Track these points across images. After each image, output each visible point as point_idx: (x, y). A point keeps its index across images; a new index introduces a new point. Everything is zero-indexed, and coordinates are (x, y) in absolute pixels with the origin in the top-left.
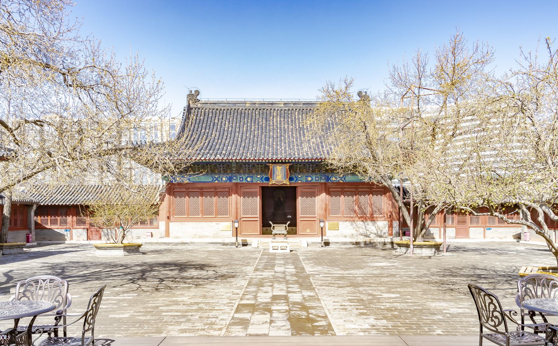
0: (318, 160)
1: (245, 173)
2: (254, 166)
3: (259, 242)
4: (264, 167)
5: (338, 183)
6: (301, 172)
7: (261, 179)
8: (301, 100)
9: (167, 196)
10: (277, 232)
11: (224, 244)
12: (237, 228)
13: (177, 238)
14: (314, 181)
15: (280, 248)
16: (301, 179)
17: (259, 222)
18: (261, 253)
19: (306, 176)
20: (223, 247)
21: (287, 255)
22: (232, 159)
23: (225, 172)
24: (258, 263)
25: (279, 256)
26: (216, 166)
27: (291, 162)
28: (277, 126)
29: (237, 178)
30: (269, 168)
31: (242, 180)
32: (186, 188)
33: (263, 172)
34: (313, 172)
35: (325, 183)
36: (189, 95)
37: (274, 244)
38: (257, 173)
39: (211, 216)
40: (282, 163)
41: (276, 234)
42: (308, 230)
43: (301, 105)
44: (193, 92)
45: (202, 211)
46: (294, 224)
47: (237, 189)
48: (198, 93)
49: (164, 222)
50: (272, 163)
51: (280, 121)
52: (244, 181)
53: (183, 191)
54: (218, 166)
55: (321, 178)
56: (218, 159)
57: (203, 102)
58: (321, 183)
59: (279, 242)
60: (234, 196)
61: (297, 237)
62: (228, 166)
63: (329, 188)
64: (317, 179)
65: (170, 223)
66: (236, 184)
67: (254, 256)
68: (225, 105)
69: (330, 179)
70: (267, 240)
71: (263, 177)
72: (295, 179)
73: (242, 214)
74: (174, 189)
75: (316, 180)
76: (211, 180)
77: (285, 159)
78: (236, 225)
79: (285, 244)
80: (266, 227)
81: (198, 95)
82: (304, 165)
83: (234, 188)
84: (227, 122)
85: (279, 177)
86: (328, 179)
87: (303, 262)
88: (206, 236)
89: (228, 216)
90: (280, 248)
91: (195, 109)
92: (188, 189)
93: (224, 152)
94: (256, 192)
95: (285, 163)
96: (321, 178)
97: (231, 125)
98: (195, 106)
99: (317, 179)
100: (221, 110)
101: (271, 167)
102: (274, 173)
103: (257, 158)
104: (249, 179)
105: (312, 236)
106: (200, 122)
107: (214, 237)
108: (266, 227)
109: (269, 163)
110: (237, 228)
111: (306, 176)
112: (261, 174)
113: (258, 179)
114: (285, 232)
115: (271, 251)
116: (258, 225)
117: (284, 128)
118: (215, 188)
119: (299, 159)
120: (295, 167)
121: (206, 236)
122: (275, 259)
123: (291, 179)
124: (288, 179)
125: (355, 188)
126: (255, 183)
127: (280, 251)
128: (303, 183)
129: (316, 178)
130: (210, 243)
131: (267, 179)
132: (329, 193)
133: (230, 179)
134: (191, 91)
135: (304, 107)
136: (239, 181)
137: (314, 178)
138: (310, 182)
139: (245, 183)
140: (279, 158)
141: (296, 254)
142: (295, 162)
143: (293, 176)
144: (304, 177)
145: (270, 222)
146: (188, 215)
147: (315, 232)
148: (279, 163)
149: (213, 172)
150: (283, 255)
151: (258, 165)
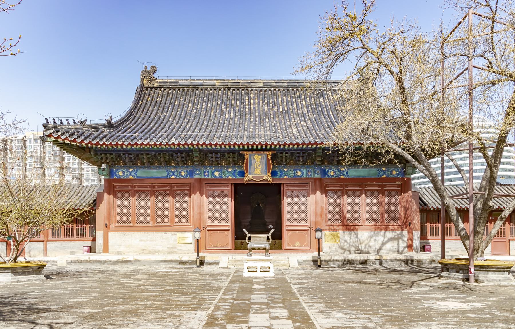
0: (312, 145)
1: (211, 165)
2: (223, 156)
3: (226, 260)
4: (236, 156)
5: (338, 179)
6: (287, 164)
7: (234, 173)
8: (285, 79)
9: (106, 195)
10: (255, 246)
11: (181, 263)
12: (198, 240)
13: (119, 253)
14: (305, 176)
15: (259, 270)
16: (287, 173)
18: (230, 278)
19: (294, 170)
20: (179, 266)
21: (270, 281)
22: (192, 144)
23: (185, 164)
24: (221, 300)
25: (259, 283)
26: (172, 156)
27: (275, 149)
28: (254, 108)
29: (201, 173)
30: (244, 158)
31: (208, 175)
32: (132, 187)
33: (235, 164)
34: (304, 164)
35: (320, 180)
36: (143, 72)
37: (251, 264)
38: (228, 165)
39: (165, 224)
40: (262, 150)
41: (253, 249)
42: (298, 244)
43: (286, 84)
44: (149, 69)
45: (153, 217)
46: (278, 236)
47: (201, 186)
48: (154, 69)
49: (102, 232)
50: (248, 150)
51: (259, 102)
52: (210, 177)
53: (127, 191)
54: (175, 155)
55: (314, 172)
56: (173, 144)
57: (161, 80)
58: (315, 179)
59: (258, 262)
60: (196, 197)
61: (283, 252)
62: (189, 155)
63: (326, 186)
64: (309, 173)
65: (110, 235)
66: (200, 180)
67: (216, 284)
68: (189, 84)
69: (326, 173)
70: (241, 256)
71: (235, 171)
72: (279, 174)
73: (207, 221)
74: (115, 187)
75: (308, 175)
76: (165, 175)
77: (266, 144)
78: (197, 235)
79: (267, 264)
80: (240, 240)
81: (155, 72)
82: (292, 154)
83: (197, 185)
84: (190, 105)
85: (258, 170)
86: (324, 173)
87: (300, 298)
88: (158, 252)
89: (189, 224)
90: (259, 270)
91: (151, 89)
92: (135, 187)
93: (182, 136)
94: (226, 191)
95: (266, 150)
96: (314, 172)
97: (195, 106)
99: (309, 173)
100: (184, 90)
101: (246, 157)
102: (251, 165)
103: (226, 143)
104: (216, 174)
105: (303, 252)
106: (155, 104)
107: (169, 253)
108: (240, 240)
109: (244, 150)
110: (198, 240)
111: (294, 170)
112: (233, 167)
113: (230, 174)
114: (268, 246)
115: (246, 274)
116: (230, 235)
117: (264, 110)
118: (171, 186)
119: (285, 144)
120: (281, 156)
121: (158, 252)
122: (250, 291)
123: (274, 173)
124: (270, 174)
125: (361, 186)
126: (225, 180)
127: (259, 274)
128: (291, 179)
129: (308, 172)
130: (162, 261)
131: (242, 174)
132: (325, 192)
133: (192, 173)
134: (146, 68)
135: (290, 86)
136: (203, 177)
138: (300, 178)
139: (212, 179)
140: (257, 143)
141: (285, 279)
142: (280, 149)
143: (277, 169)
144: (292, 171)
145: (245, 230)
146: (134, 222)
147: (307, 245)
148: (257, 149)
149: (168, 164)
150: (266, 281)
151: (229, 154)
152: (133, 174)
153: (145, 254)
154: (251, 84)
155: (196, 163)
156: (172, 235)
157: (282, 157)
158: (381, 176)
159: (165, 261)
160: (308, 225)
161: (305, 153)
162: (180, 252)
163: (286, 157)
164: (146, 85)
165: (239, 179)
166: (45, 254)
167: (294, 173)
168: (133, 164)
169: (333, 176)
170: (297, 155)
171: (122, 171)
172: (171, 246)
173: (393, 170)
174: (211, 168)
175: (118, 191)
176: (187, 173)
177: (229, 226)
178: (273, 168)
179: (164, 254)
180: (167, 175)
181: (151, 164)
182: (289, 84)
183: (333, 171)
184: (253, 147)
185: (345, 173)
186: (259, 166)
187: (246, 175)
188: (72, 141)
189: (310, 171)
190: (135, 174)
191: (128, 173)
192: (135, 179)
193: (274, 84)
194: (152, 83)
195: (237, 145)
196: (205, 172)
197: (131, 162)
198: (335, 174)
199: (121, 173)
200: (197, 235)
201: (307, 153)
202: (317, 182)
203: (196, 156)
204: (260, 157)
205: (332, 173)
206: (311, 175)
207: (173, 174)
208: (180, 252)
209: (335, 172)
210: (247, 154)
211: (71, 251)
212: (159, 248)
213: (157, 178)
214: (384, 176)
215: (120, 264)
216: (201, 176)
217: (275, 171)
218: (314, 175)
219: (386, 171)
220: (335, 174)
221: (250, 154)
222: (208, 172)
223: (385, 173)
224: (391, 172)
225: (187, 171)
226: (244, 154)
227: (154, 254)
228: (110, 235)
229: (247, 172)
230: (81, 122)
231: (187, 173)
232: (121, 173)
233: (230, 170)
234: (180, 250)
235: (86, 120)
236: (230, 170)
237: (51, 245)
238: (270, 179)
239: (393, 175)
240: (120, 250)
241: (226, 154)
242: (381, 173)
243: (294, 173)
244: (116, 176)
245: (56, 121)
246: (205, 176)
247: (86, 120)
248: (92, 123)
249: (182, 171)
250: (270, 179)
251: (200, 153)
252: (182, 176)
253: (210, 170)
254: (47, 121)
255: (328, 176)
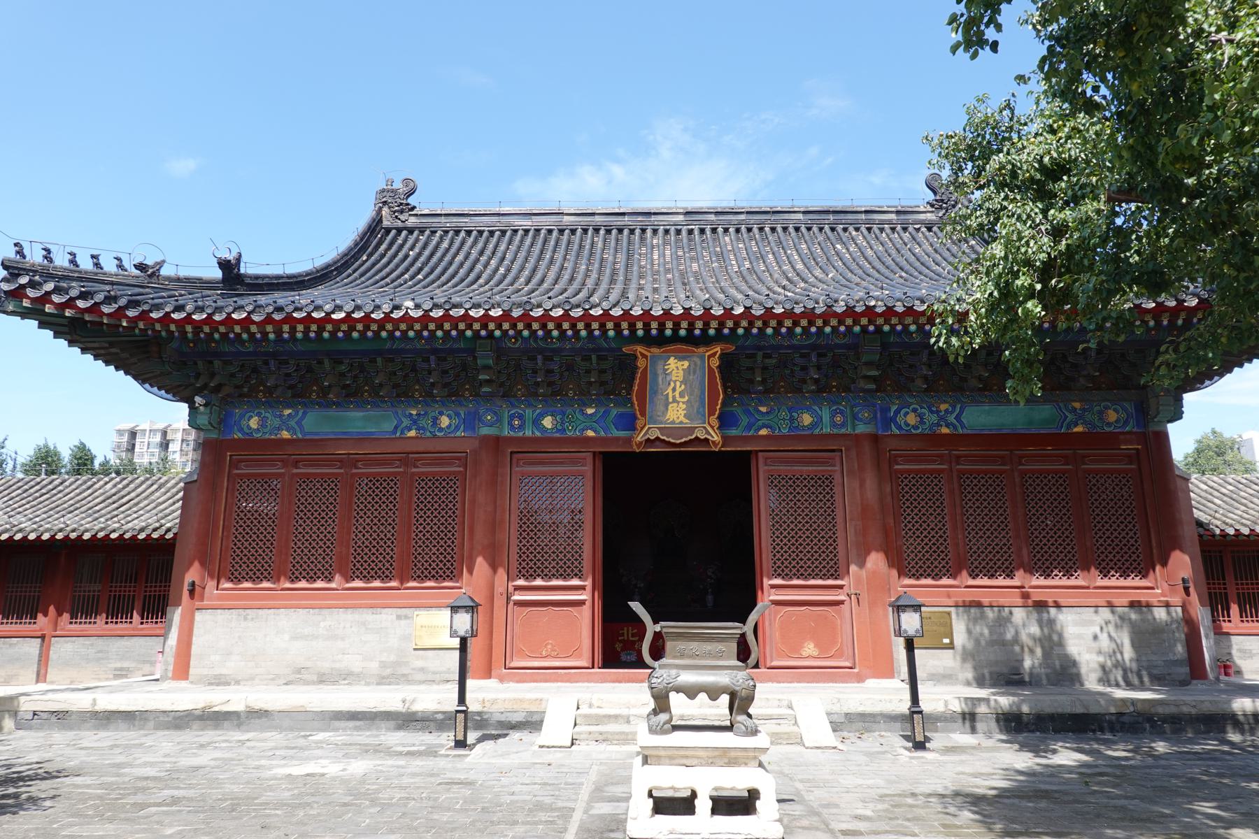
5: (934, 439)
6: (767, 391)
16: (764, 423)
17: (586, 609)
19: (790, 410)
31: (521, 427)
32: (285, 463)
35: (875, 439)
36: (383, 191)
37: (673, 780)
40: (691, 340)
42: (810, 649)
43: (742, 217)
50: (648, 341)
52: (528, 433)
55: (855, 417)
57: (426, 212)
58: (857, 438)
63: (893, 460)
64: (838, 419)
65: (199, 616)
66: (496, 443)
69: (893, 419)
71: (606, 413)
72: (745, 420)
74: (234, 464)
75: (834, 425)
81: (411, 193)
85: (678, 402)
86: (888, 422)
90: (703, 804)
92: (296, 464)
95: (705, 340)
96: (855, 417)
98: (400, 224)
99: (838, 419)
101: (641, 363)
107: (382, 680)
112: (598, 404)
113: (592, 423)
123: (725, 421)
124: (714, 420)
128: (784, 437)
131: (630, 423)
133: (471, 421)
136: (506, 432)
137: (826, 415)
139: (533, 440)
143: (736, 408)
145: (636, 606)
147: (838, 654)
148: (675, 338)
152: (292, 423)
153: (307, 683)
154: (653, 218)
155: (486, 389)
156: (399, 617)
157: (751, 369)
158: (1069, 427)
159: (354, 716)
160: (841, 587)
161: (824, 355)
162: (420, 677)
163: (765, 368)
164: (386, 223)
165: (617, 439)
166: (41, 677)
167: (792, 419)
168: (294, 396)
169: (915, 427)
170: (798, 360)
171: (259, 415)
172: (393, 658)
173: (1107, 408)
174: (530, 405)
175: (241, 476)
176: (455, 421)
177: (583, 588)
178: (723, 403)
179: (368, 684)
180: (396, 428)
181: (351, 395)
182: (750, 217)
183: (915, 410)
184: (662, 327)
185: (952, 418)
186: (681, 395)
187: (639, 423)
188: (87, 310)
189: (842, 413)
190: (298, 423)
191: (277, 422)
192: (298, 440)
193: (712, 217)
194: (402, 217)
195: (612, 318)
196: (512, 417)
197: (291, 387)
198: (922, 422)
199: (254, 423)
200: (463, 622)
201: (830, 355)
202: (867, 448)
203: (487, 367)
204: (686, 364)
205: (912, 419)
206: (843, 425)
207: (415, 422)
208: (420, 677)
209: (921, 416)
210: (644, 356)
211: (119, 665)
212: (354, 663)
213: (363, 439)
214: (1079, 429)
215: (196, 724)
216: (501, 430)
217: (732, 414)
218: (854, 427)
219: (1084, 410)
220: (922, 422)
221: (653, 357)
222: (521, 417)
223: (1081, 417)
224: (1101, 413)
225: (458, 414)
226: (634, 357)
227: (335, 682)
228: (199, 616)
229: (643, 414)
230: (141, 267)
231: (455, 421)
232: (254, 423)
233: (590, 411)
234: (422, 670)
235: (161, 264)
236: (590, 411)
237: (62, 648)
238: (715, 437)
239: (1109, 424)
240: (224, 671)
241: (578, 359)
242: (1070, 417)
243: (792, 419)
244: (241, 430)
245: (102, 261)
246: (512, 427)
247: (161, 264)
248: (183, 273)
249: (441, 414)
250: (715, 437)
251: (498, 358)
252: (441, 429)
253: (529, 412)
254: (20, 252)
255: (899, 428)
